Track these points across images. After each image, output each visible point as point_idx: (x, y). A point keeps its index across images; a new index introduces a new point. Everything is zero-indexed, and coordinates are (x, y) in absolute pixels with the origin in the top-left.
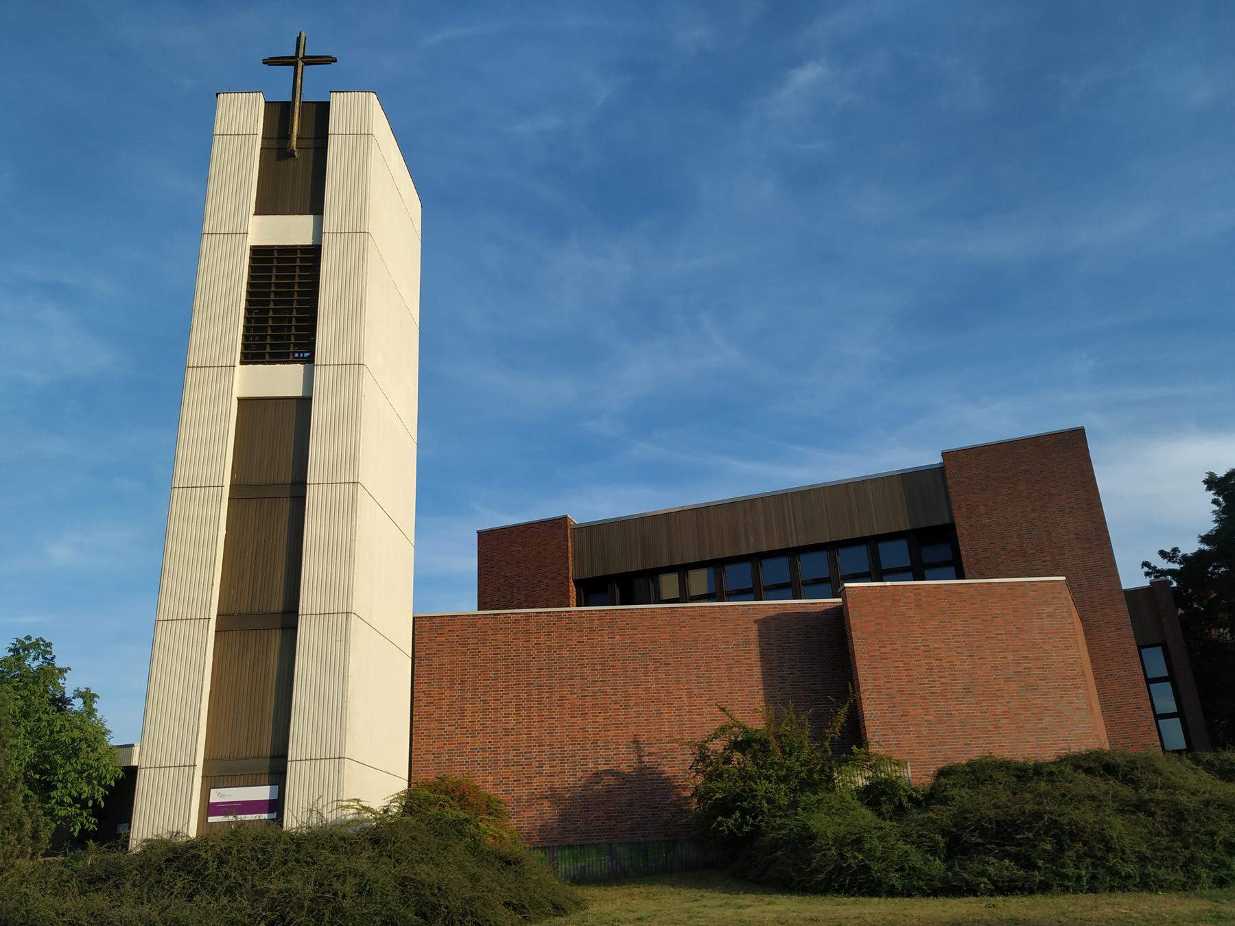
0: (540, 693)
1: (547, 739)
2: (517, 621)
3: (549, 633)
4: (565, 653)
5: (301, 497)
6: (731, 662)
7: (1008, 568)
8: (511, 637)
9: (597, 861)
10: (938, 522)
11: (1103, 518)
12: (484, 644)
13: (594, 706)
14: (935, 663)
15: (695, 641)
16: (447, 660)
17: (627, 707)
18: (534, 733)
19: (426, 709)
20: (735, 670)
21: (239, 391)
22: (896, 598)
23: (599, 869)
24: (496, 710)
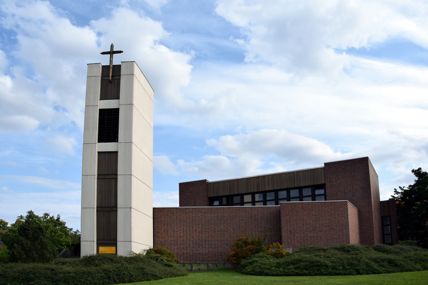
0: (190, 228)
1: (192, 239)
2: (183, 210)
3: (193, 213)
4: (197, 218)
5: (99, 178)
6: (246, 221)
7: (339, 196)
9: (203, 267)
10: (321, 183)
11: (370, 183)
12: (174, 215)
13: (205, 231)
14: (305, 222)
15: (236, 216)
16: (163, 219)
17: (215, 232)
20: (247, 224)
21: (97, 150)
22: (296, 206)
24: (177, 231)
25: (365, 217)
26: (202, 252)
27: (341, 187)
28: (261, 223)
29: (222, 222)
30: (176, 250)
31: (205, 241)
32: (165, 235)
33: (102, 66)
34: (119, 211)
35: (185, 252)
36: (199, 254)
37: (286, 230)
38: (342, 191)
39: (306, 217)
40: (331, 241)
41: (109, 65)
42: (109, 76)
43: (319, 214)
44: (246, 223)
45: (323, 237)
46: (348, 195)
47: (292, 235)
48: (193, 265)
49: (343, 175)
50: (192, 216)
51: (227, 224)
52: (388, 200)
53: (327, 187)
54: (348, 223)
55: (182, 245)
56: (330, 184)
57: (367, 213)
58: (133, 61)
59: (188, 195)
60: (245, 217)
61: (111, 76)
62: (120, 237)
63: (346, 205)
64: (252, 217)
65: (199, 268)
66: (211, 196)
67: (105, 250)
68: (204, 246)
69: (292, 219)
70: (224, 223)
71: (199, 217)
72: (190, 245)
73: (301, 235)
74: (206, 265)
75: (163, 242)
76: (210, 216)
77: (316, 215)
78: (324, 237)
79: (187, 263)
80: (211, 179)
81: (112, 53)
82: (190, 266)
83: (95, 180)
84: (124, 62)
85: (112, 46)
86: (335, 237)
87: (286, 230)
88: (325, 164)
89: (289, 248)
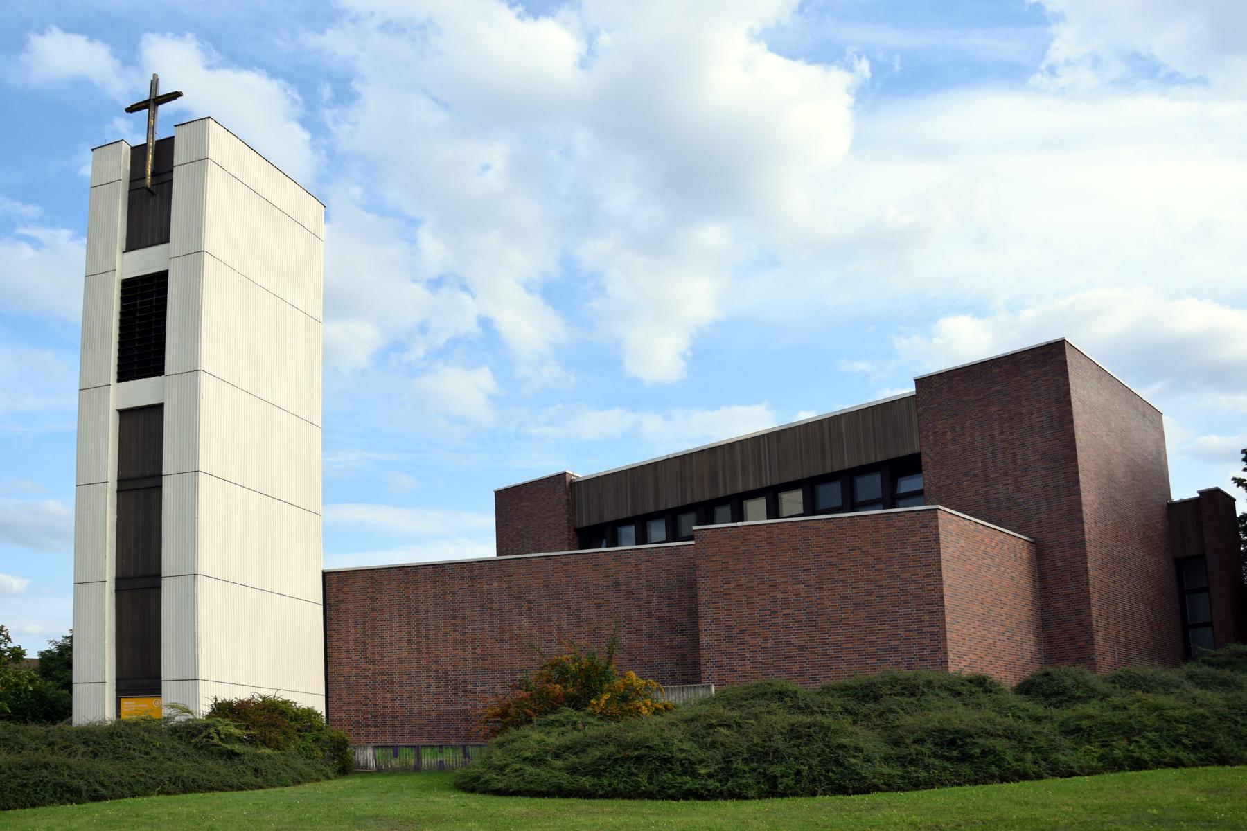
0: (427, 631)
1: (434, 667)
3: (435, 582)
4: (449, 598)
7: (969, 494)
8: (402, 587)
12: (381, 592)
13: (473, 640)
14: (779, 595)
15: (567, 584)
16: (351, 606)
17: (502, 641)
18: (423, 662)
19: (337, 643)
22: (746, 537)
23: (454, 763)
25: (1059, 564)
26: (466, 707)
27: (974, 459)
28: (649, 603)
29: (525, 608)
30: (389, 704)
31: (474, 670)
32: (357, 658)
33: (132, 148)
34: (166, 584)
35: (416, 710)
36: (457, 713)
37: (713, 627)
38: (975, 475)
39: (783, 577)
40: (875, 660)
41: (145, 142)
42: (144, 178)
43: (831, 564)
44: (599, 606)
45: (844, 646)
46: (996, 487)
47: (736, 641)
48: (423, 751)
49: (980, 415)
50: (433, 590)
51: (539, 613)
52: (1198, 495)
53: (927, 462)
54: (942, 592)
55: (408, 688)
56: (937, 454)
57: (1067, 548)
58: (205, 118)
59: (519, 527)
60: (597, 585)
61: (151, 173)
62: (169, 667)
63: (933, 524)
64: (618, 584)
65: (440, 762)
66: (581, 526)
67: (134, 707)
68: (470, 687)
69: (732, 585)
70: (530, 609)
71: (454, 594)
72: (429, 686)
73: (766, 640)
74: (460, 750)
75: (353, 679)
76: (485, 587)
77: (819, 568)
78: (850, 646)
79: (405, 746)
80: (580, 470)
81: (155, 101)
82: (413, 754)
83: (108, 495)
84: (183, 126)
85: (155, 83)
86: (892, 643)
87: (713, 627)
88: (919, 382)
89: (705, 689)
